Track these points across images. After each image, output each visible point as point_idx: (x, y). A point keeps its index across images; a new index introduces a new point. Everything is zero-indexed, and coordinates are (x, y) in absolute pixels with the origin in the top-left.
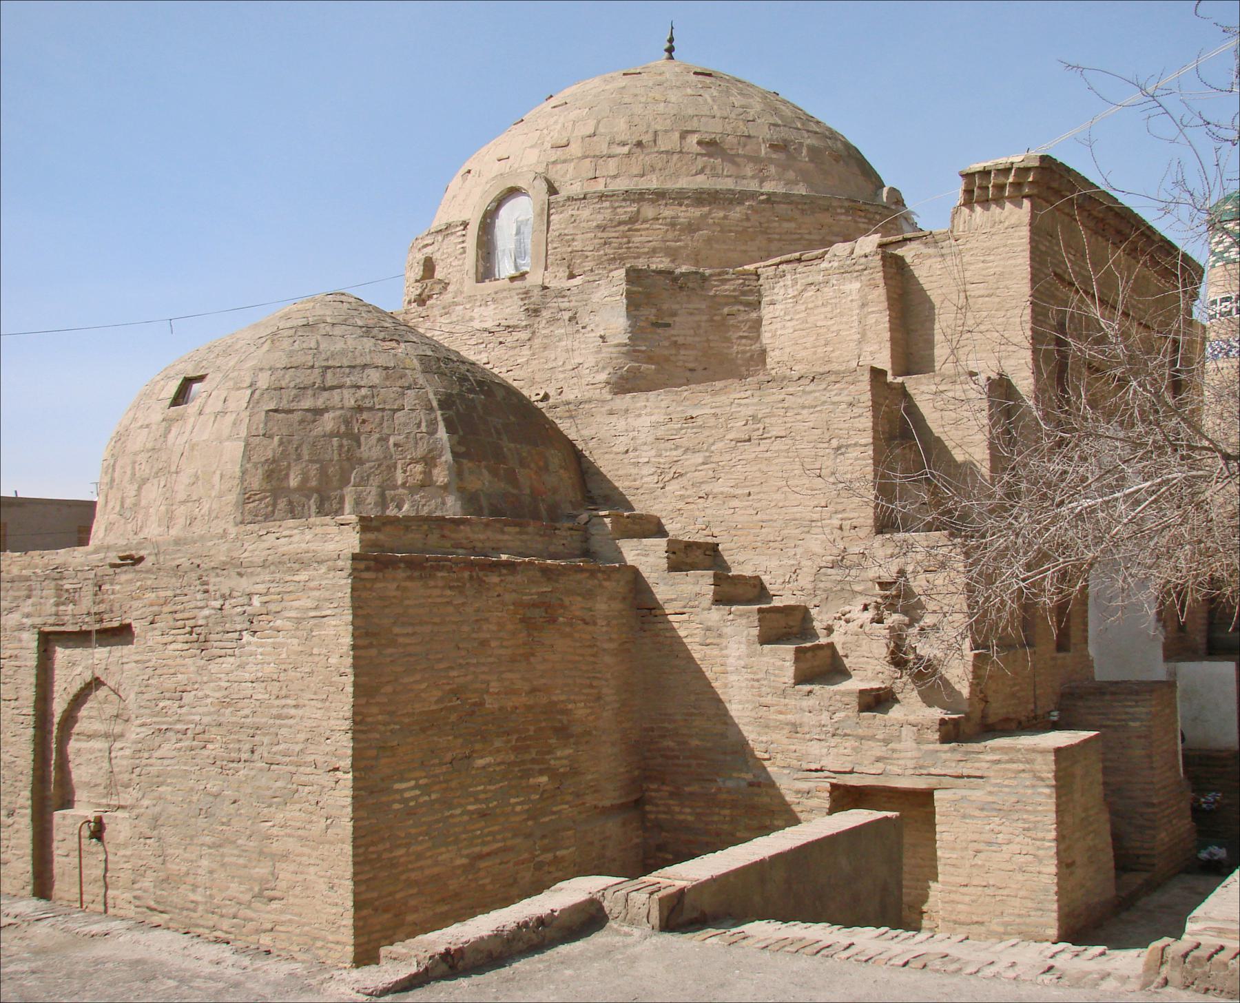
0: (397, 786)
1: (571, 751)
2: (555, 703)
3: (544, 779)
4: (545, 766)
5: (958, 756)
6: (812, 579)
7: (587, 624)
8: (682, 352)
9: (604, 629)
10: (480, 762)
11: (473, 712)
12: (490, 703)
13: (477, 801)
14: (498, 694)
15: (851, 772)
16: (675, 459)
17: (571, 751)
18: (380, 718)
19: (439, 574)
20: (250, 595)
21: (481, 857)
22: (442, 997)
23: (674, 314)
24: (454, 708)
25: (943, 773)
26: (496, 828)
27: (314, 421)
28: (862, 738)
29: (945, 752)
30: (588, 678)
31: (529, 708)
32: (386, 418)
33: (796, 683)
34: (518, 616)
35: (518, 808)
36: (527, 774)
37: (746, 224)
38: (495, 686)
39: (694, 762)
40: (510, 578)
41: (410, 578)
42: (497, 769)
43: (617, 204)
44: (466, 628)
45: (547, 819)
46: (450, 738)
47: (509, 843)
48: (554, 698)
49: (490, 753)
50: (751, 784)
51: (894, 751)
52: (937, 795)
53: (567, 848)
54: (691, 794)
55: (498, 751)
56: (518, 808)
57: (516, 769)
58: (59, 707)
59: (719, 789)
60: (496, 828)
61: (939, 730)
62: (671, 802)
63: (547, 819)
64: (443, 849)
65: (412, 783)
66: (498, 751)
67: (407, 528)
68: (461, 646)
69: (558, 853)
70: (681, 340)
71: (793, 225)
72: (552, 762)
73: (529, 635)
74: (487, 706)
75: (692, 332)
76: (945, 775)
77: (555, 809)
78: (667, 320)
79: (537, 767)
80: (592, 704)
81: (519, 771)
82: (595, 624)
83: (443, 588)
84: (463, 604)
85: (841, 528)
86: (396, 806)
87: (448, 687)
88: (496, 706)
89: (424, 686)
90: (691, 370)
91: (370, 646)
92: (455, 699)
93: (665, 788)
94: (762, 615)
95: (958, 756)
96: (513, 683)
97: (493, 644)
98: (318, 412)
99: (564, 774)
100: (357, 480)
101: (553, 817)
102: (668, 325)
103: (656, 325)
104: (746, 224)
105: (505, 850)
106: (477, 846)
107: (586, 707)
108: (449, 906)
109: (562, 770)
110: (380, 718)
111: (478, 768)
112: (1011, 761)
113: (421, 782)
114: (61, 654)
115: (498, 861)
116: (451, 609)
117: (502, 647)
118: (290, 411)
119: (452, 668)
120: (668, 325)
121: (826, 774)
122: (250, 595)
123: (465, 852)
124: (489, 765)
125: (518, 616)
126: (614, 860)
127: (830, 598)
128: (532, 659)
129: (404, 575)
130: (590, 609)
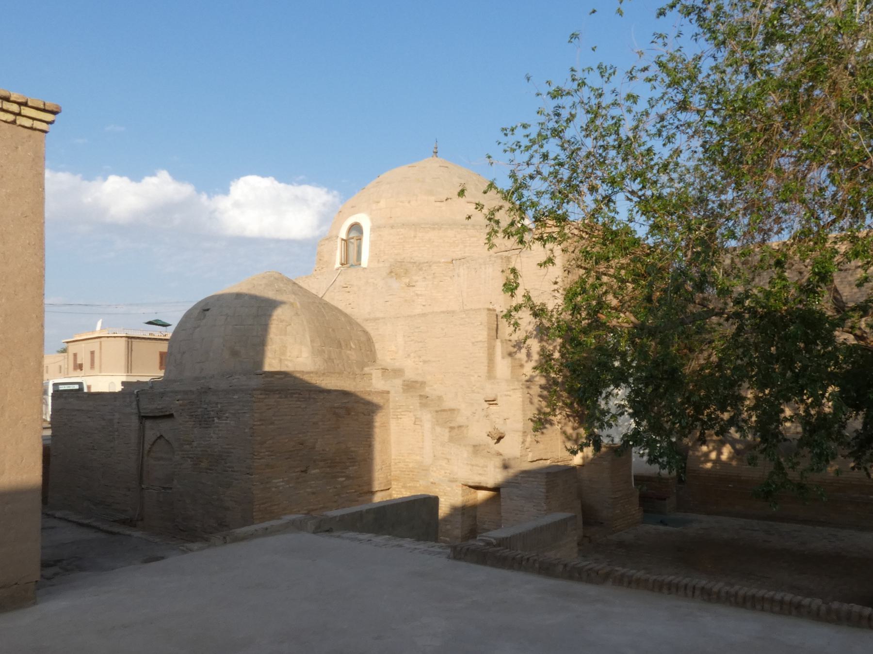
0: (274, 481)
7: (365, 415)
8: (420, 298)
18: (267, 453)
19: (294, 396)
20: (217, 403)
23: (417, 281)
28: (472, 465)
35: (331, 491)
37: (455, 239)
39: (411, 473)
41: (280, 398)
43: (398, 230)
45: (344, 495)
50: (432, 483)
51: (485, 471)
54: (410, 486)
58: (147, 446)
59: (420, 485)
62: (402, 490)
63: (344, 495)
65: (281, 480)
70: (419, 293)
71: (475, 239)
75: (424, 289)
77: (348, 491)
78: (414, 284)
83: (296, 401)
86: (273, 489)
89: (287, 440)
90: (424, 306)
91: (262, 425)
93: (400, 484)
101: (347, 495)
102: (414, 286)
103: (409, 286)
104: (455, 239)
110: (267, 453)
112: (529, 477)
113: (285, 479)
114: (148, 424)
117: (397, 415)
120: (414, 286)
122: (217, 403)
123: (305, 508)
129: (278, 396)
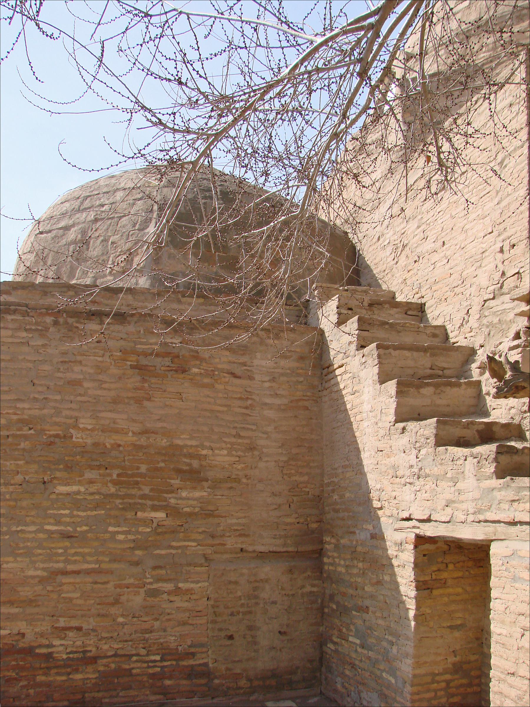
1: (205, 494)
2: (180, 448)
3: (161, 515)
4: (165, 503)
5: (510, 494)
6: (478, 316)
9: (267, 385)
10: (62, 489)
11: (52, 443)
12: (77, 437)
13: (58, 523)
14: (92, 430)
15: (428, 520)
16: (403, 232)
17: (205, 494)
21: (65, 573)
22: (283, 705)
24: (26, 437)
25: (496, 518)
26: (87, 550)
27: (64, 235)
29: (500, 490)
30: (235, 428)
31: (138, 448)
32: (113, 224)
33: (396, 421)
34: (129, 363)
36: (134, 508)
38: (86, 422)
40: (118, 327)
42: (89, 498)
44: (47, 367)
46: (21, 463)
47: (104, 566)
48: (179, 442)
49: (80, 483)
52: (495, 549)
53: (197, 582)
55: (91, 482)
56: (121, 537)
57: (118, 501)
60: (87, 550)
61: (496, 460)
64: (11, 559)
66: (91, 482)
67: (45, 293)
68: (35, 381)
69: (180, 585)
72: (173, 501)
73: (144, 380)
74: (74, 439)
76: (499, 522)
79: (149, 503)
80: (240, 453)
81: (121, 504)
82: (251, 378)
84: (44, 346)
85: (502, 251)
87: (15, 417)
88: (89, 441)
92: (27, 428)
94: (382, 351)
95: (510, 494)
96: (114, 423)
97: (86, 385)
98: (67, 228)
99: (190, 514)
100: (80, 275)
105: (99, 572)
106: (58, 562)
107: (229, 455)
108: (21, 610)
109: (185, 509)
111: (58, 494)
115: (91, 580)
116: (25, 349)
118: (50, 231)
119: (19, 400)
121: (413, 523)
124: (78, 493)
125: (129, 363)
126: (274, 603)
127: (492, 334)
128: (146, 403)
130: (244, 364)
